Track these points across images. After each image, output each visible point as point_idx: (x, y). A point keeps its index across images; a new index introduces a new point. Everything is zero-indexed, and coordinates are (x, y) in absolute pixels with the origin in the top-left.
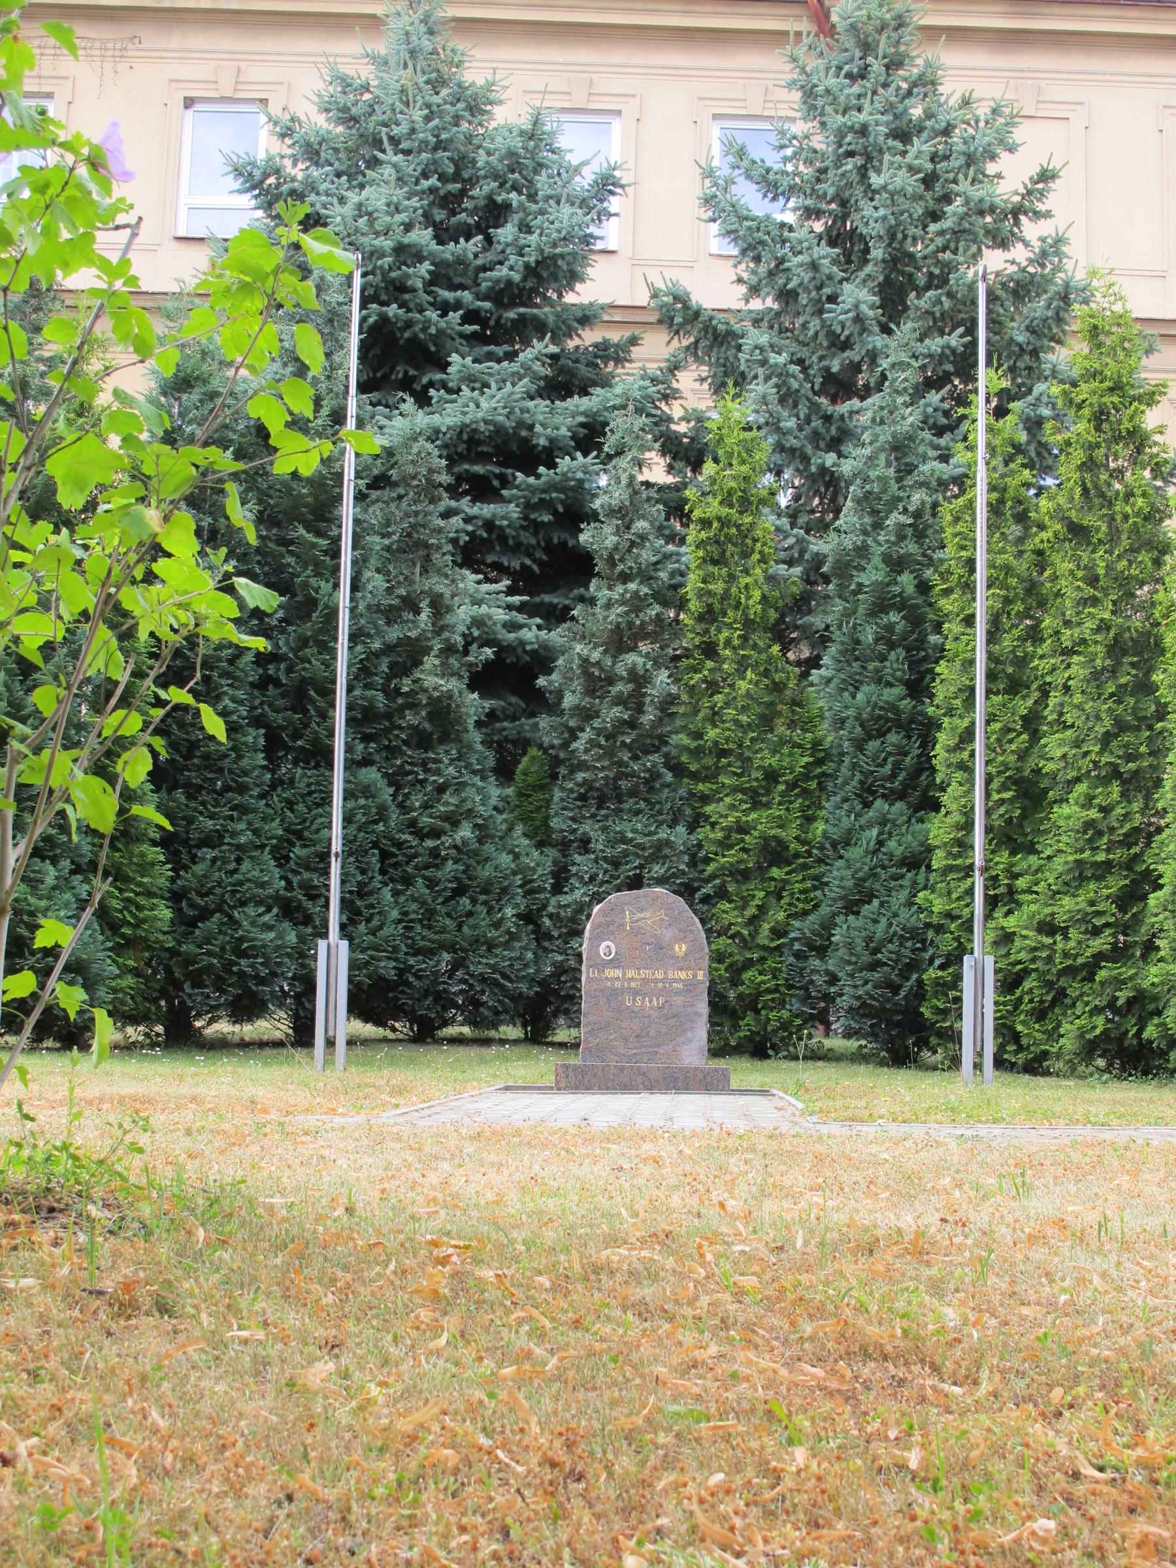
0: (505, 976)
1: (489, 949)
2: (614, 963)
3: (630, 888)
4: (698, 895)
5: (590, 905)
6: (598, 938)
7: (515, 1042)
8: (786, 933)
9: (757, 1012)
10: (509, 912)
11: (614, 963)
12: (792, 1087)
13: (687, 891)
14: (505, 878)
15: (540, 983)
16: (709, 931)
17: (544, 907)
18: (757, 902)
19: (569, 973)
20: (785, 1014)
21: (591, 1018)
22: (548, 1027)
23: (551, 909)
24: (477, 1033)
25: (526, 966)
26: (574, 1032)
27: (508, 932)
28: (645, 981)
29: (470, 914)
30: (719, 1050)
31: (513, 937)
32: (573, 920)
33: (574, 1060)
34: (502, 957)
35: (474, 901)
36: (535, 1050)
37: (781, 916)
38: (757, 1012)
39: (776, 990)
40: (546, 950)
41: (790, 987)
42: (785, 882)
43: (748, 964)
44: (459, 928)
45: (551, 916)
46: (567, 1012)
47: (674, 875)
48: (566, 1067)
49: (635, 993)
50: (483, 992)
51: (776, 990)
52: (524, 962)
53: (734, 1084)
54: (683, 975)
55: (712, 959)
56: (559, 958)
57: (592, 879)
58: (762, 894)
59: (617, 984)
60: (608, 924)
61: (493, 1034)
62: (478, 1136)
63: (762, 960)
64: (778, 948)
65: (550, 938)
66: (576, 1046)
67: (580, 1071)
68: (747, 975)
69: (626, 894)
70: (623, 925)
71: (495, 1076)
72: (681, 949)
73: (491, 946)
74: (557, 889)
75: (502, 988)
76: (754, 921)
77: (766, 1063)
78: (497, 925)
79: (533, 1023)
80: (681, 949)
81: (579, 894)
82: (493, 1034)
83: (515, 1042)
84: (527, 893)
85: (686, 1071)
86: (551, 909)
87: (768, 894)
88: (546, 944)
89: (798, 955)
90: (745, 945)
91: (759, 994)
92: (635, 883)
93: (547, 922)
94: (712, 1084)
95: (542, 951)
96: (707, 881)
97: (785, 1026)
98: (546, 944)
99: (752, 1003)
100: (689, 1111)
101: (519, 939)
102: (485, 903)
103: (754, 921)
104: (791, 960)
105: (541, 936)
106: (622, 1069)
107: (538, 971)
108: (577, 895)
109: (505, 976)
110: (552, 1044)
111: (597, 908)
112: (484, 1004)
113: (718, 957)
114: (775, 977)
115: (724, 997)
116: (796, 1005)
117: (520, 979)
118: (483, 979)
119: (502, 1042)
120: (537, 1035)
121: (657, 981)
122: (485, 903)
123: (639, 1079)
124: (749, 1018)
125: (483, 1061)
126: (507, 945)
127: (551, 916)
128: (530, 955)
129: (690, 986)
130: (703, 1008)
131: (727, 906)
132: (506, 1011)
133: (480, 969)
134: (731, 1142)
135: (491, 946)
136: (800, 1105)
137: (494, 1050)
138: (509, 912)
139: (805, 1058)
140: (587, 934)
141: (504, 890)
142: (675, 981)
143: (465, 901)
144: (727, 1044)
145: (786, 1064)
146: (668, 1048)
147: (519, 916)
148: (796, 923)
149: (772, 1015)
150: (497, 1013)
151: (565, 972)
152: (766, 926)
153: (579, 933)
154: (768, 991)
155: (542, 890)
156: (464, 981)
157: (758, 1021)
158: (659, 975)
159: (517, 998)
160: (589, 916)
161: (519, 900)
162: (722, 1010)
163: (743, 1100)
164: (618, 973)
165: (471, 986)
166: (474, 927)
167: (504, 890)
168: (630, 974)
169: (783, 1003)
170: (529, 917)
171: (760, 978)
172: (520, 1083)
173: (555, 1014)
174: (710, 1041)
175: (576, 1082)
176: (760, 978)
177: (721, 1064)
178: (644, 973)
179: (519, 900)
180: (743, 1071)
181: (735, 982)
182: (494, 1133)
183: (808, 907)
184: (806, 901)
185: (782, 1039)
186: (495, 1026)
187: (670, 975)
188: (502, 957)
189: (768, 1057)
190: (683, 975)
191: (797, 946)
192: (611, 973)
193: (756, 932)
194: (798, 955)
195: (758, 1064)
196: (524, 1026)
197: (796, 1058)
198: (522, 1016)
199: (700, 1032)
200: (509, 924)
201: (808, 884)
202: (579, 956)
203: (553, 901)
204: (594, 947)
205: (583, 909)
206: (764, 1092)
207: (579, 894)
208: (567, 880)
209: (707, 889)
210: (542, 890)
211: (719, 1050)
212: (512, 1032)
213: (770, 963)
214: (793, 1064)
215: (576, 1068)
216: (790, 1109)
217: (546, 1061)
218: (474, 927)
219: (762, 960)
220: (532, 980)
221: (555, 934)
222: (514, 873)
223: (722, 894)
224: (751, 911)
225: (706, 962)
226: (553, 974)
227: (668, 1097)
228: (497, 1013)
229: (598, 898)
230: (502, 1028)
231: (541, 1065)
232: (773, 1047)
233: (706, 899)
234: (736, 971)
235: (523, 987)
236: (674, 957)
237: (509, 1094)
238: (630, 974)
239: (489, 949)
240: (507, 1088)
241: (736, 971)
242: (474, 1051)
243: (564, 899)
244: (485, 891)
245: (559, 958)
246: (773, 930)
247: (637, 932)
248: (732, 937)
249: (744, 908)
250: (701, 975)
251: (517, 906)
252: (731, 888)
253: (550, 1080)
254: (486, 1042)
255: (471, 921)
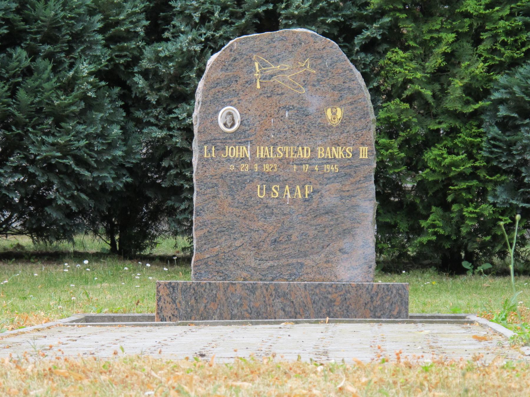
0: (80, 161)
1: (57, 123)
2: (240, 137)
3: (260, 29)
4: (358, 40)
5: (202, 56)
6: (215, 102)
7: (98, 256)
8: (487, 93)
9: (446, 207)
10: (85, 68)
11: (240, 137)
12: (497, 312)
13: (343, 34)
14: (78, 19)
15: (131, 171)
16: (375, 92)
17: (136, 60)
18: (444, 48)
19: (173, 156)
20: (487, 210)
21: (206, 217)
22: (145, 235)
23: (145, 64)
24: (42, 245)
25: (111, 146)
26: (182, 241)
27: (84, 98)
28: (284, 162)
29: (28, 72)
30: (392, 263)
31: (91, 105)
32: (178, 78)
33: (182, 278)
34: (76, 135)
35: (33, 54)
36: (127, 267)
37: (479, 68)
38: (446, 207)
39: (473, 175)
40: (139, 123)
41: (494, 170)
42: (484, 18)
43: (432, 139)
44: (13, 92)
45: (145, 74)
46: (171, 212)
47: (323, 12)
48: (172, 287)
49: (270, 180)
50: (49, 185)
51: (473, 175)
52: (107, 140)
53: (414, 309)
54: (338, 153)
55: (379, 131)
56: (159, 134)
57: (204, 19)
58: (451, 37)
59: (245, 168)
60: (229, 81)
61: (65, 245)
62: (50, 373)
63: (453, 132)
64: (475, 114)
65: (145, 105)
66: (187, 260)
67: (194, 293)
68: (431, 155)
69: (254, 37)
70: (251, 82)
71: (70, 303)
72: (335, 115)
73: (59, 119)
74: (155, 34)
75: (77, 178)
76: (439, 76)
77: (460, 280)
78: (68, 87)
79: (124, 228)
80: (335, 115)
81: (186, 41)
82: (65, 245)
83: (98, 256)
84: (111, 41)
85: (344, 290)
86: (145, 64)
87: (460, 36)
88: (139, 114)
89: (505, 125)
90: (427, 111)
91: (449, 181)
92: (268, 22)
93: (140, 81)
94: (387, 309)
95: (133, 124)
96: (372, 19)
97: (486, 226)
98: (139, 114)
99: (438, 194)
100: (352, 341)
101: (100, 108)
102: (49, 56)
103: (439, 76)
104: (495, 131)
105: (131, 102)
106: (253, 289)
107: (129, 153)
108: (184, 41)
109: (80, 161)
110: (151, 259)
111: (212, 59)
112: (51, 202)
113: (389, 129)
114: (471, 156)
115: (398, 188)
116: (502, 197)
117: (103, 165)
118: (50, 167)
119: (79, 256)
120: (129, 246)
121: (301, 162)
122: (49, 56)
123: (278, 303)
124: (435, 216)
125: (51, 283)
126: (82, 117)
127: (145, 74)
128: (116, 131)
129: (348, 168)
130: (368, 206)
131: (400, 55)
132: (83, 212)
133: (45, 152)
134: (412, 376)
135: (59, 119)
136: (509, 333)
137: (67, 267)
138: (85, 68)
139: (517, 272)
140: (199, 96)
141: (77, 38)
142: (328, 161)
143: (20, 54)
144: (403, 254)
145: (488, 281)
146: (319, 258)
147: (99, 74)
148: (501, 79)
149: (467, 211)
150: (70, 215)
151: (167, 154)
152: (458, 83)
153: (188, 98)
154: (462, 176)
155: (131, 35)
156: (24, 171)
157: (448, 221)
158: (304, 154)
159: (99, 192)
160: (200, 73)
161: (98, 50)
162: (396, 210)
163: (427, 329)
164: (245, 151)
165: (32, 177)
166: (35, 91)
167: (77, 38)
168: (262, 152)
169: (483, 194)
170: (113, 76)
171: (449, 159)
172: (106, 312)
173: (155, 216)
174: (379, 250)
175: (186, 308)
176: (449, 159)
177: (395, 281)
178: (284, 151)
179: (98, 50)
180: (426, 292)
181: (413, 165)
182: (72, 368)
183: (518, 54)
184: (515, 46)
185: (483, 246)
186: (67, 233)
187: (320, 153)
188: (76, 135)
189: (463, 271)
190: (338, 153)
191: (502, 112)
192: (235, 152)
193: (443, 91)
194: (505, 125)
195: (449, 281)
196: (110, 233)
197: (505, 273)
198: (104, 218)
199: (366, 235)
200: (86, 87)
201: (519, 21)
202: (188, 131)
203: (148, 52)
204: (210, 115)
205: (192, 63)
206: (457, 320)
207: (186, 41)
208: (168, 21)
209: (372, 31)
210: (131, 35)
211: (392, 263)
212: (92, 242)
213: (464, 136)
214: (499, 281)
215: (186, 288)
216: (496, 339)
217: (144, 282)
218: (35, 91)
219: (453, 132)
220: (120, 167)
221: (153, 99)
222: (91, 12)
223: (393, 37)
224: (435, 61)
225: (372, 135)
226: (150, 158)
227: (321, 327)
228: (70, 215)
229: (212, 45)
230: (77, 238)
231: (138, 286)
232: (469, 257)
233: (370, 46)
234: (414, 153)
235: (108, 177)
236: (325, 128)
237: (89, 328)
238: (262, 152)
239: (57, 123)
240: (88, 320)
241: (414, 153)
242: (38, 271)
243: (165, 49)
244: (50, 39)
245: (159, 134)
246: (468, 89)
247: (271, 92)
248: (409, 100)
249: (425, 57)
250: (364, 152)
251: (96, 59)
252: (407, 28)
253: (150, 306)
254: (56, 257)
255: (30, 83)
